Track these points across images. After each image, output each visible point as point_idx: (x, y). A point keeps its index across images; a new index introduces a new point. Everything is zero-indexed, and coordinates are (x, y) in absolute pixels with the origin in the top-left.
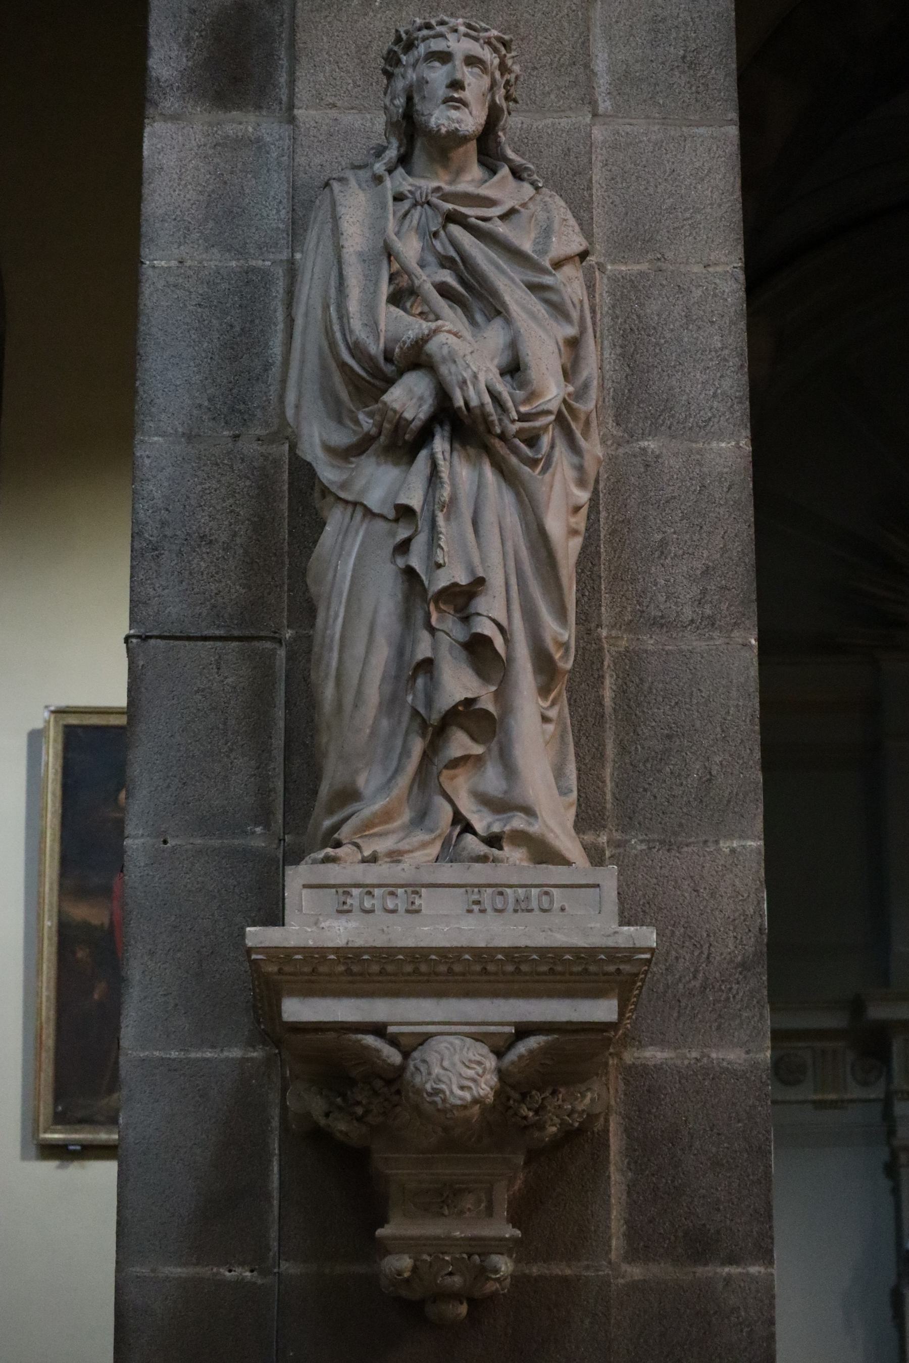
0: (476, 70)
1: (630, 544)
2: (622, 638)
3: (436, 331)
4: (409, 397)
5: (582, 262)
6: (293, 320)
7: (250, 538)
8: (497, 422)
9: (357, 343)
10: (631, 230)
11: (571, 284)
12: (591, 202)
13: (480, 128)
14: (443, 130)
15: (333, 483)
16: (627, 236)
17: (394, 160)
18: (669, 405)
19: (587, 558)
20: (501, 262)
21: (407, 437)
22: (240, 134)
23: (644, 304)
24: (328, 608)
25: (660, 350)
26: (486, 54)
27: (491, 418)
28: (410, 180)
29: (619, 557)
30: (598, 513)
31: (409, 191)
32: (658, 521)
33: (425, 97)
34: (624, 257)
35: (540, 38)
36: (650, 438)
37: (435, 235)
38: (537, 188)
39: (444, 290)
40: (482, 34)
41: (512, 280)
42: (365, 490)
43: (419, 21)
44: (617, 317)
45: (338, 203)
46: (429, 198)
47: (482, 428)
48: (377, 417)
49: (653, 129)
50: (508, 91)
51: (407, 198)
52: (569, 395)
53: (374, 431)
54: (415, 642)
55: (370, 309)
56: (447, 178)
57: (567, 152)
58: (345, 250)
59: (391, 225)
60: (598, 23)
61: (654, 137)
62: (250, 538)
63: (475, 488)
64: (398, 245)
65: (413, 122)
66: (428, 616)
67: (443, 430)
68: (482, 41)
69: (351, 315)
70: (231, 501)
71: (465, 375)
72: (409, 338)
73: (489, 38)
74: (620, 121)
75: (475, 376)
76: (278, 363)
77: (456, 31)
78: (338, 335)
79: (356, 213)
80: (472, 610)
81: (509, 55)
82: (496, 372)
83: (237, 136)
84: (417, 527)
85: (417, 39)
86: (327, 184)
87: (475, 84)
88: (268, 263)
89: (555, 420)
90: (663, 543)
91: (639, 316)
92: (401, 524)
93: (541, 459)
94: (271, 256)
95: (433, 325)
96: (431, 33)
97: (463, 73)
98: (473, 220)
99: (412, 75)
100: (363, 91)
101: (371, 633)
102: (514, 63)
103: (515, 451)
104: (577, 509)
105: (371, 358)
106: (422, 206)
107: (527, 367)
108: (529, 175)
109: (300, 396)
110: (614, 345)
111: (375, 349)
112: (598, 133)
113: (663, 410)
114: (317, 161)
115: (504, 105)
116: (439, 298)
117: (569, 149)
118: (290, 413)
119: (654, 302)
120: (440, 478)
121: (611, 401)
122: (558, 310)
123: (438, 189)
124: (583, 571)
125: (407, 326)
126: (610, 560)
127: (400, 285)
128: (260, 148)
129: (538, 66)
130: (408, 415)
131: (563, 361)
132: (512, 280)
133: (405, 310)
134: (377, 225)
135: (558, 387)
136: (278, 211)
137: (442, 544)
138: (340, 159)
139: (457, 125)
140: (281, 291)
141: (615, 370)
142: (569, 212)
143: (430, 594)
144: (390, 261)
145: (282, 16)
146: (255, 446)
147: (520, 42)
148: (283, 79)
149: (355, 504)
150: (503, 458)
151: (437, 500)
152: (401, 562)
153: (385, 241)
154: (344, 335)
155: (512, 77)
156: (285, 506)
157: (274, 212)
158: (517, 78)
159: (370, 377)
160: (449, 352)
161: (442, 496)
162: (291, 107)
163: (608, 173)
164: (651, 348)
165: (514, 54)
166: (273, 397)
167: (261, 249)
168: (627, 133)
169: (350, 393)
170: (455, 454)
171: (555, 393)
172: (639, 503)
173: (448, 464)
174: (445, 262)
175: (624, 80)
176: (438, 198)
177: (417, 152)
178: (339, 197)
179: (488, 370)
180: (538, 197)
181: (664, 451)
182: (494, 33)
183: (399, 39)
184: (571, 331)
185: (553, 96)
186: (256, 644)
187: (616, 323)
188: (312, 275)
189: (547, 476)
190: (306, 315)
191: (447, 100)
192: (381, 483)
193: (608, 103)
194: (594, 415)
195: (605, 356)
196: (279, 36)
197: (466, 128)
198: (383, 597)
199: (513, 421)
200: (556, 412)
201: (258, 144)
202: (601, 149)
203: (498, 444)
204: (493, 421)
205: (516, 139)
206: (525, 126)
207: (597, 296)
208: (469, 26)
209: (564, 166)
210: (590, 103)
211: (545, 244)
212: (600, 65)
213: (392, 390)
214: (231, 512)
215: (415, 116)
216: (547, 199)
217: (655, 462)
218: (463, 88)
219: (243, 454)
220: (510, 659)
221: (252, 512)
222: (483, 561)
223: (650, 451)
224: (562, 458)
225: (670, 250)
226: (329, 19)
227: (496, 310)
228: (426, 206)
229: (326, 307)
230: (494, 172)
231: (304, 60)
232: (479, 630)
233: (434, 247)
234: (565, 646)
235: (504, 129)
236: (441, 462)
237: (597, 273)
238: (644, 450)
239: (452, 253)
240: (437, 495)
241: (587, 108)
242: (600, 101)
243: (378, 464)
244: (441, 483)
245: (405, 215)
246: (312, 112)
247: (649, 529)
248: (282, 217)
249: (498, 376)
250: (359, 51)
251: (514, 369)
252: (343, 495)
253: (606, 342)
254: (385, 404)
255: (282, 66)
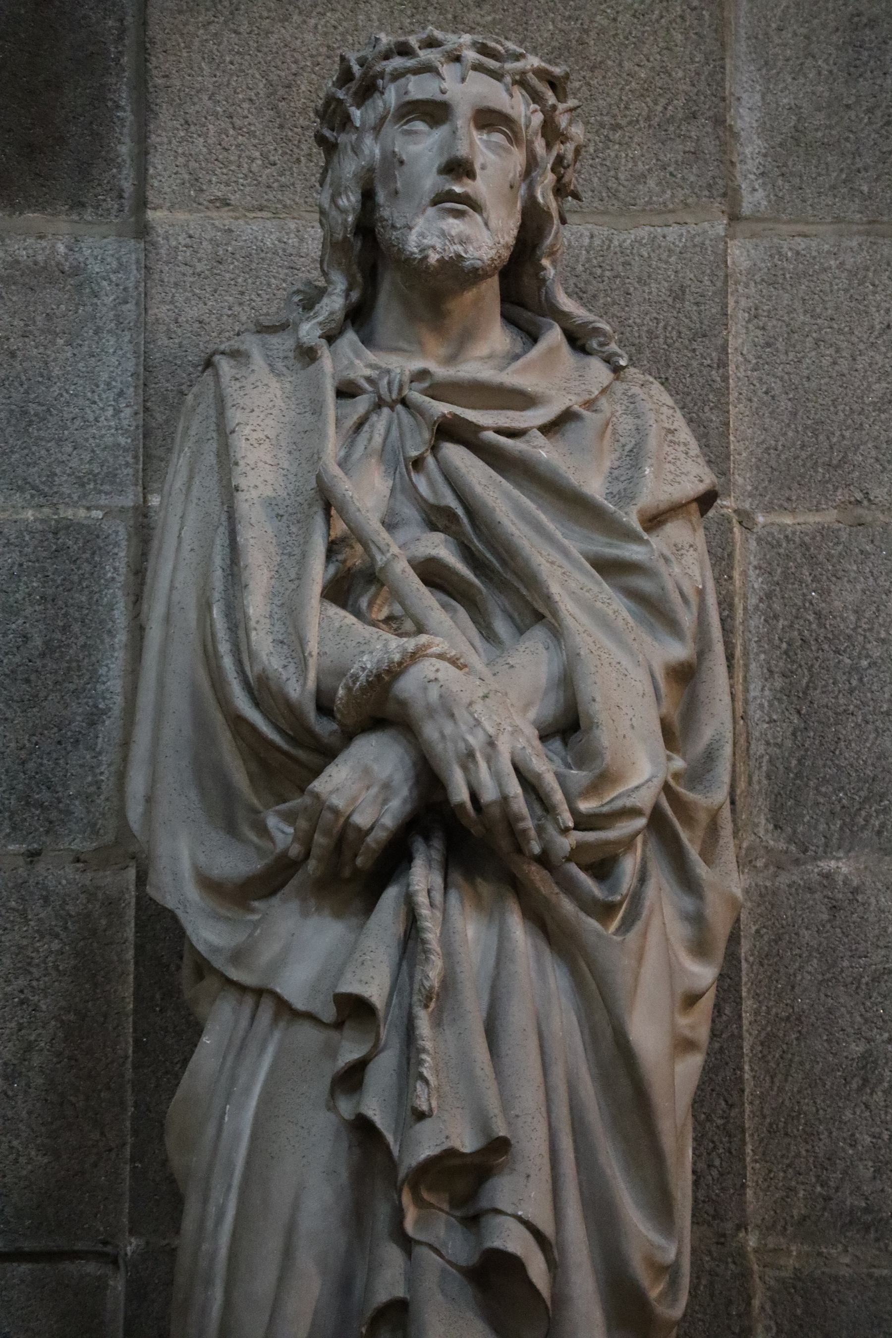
0: (497, 137)
1: (801, 1063)
2: (789, 1252)
3: (415, 656)
4: (363, 784)
5: (702, 516)
6: (142, 628)
7: (59, 1054)
8: (533, 833)
9: (264, 680)
10: (803, 447)
11: (681, 559)
12: (724, 392)
13: (506, 254)
14: (433, 258)
15: (216, 950)
16: (796, 458)
17: (340, 316)
18: (877, 788)
19: (716, 1091)
20: (543, 517)
21: (359, 861)
22: (40, 258)
23: (829, 592)
24: (205, 1201)
25: (861, 680)
26: (518, 106)
27: (521, 825)
28: (370, 356)
29: (781, 1090)
30: (739, 1001)
31: (369, 379)
32: (859, 1019)
33: (397, 193)
34: (789, 499)
35: (627, 65)
36: (841, 855)
37: (417, 464)
38: (617, 370)
39: (432, 574)
40: (509, 66)
41: (565, 553)
42: (278, 964)
43: (385, 39)
44: (776, 617)
45: (229, 402)
46: (406, 392)
47: (504, 844)
48: (303, 824)
49: (849, 243)
50: (560, 179)
51: (362, 391)
52: (676, 776)
53: (295, 850)
54: (373, 1269)
55: (290, 614)
56: (443, 351)
57: (679, 294)
58: (241, 496)
59: (332, 446)
60: (742, 32)
61: (850, 262)
62: (59, 1054)
63: (492, 962)
64: (345, 486)
65: (375, 239)
66: (399, 1214)
67: (429, 846)
68: (508, 79)
69: (253, 623)
70: (21, 982)
71: (471, 739)
72: (364, 669)
73: (523, 73)
74: (784, 228)
75: (491, 743)
76: (116, 711)
77: (458, 59)
78: (228, 662)
79: (265, 422)
80: (484, 1204)
81: (561, 107)
82: (532, 733)
83: (36, 263)
84: (378, 1039)
85: (382, 75)
86: (209, 364)
87: (495, 165)
88: (98, 514)
89: (648, 826)
90: (868, 1061)
91: (818, 614)
92: (347, 1031)
93: (621, 903)
94: (103, 501)
95: (411, 644)
96: (410, 63)
97: (472, 144)
98: (490, 435)
99: (372, 148)
100: (282, 174)
101: (288, 1253)
102: (570, 123)
103: (570, 887)
104: (691, 1000)
105: (292, 709)
106: (392, 408)
107: (593, 725)
108: (602, 345)
109: (153, 782)
110: (771, 671)
111: (299, 690)
112: (740, 254)
113: (866, 800)
114: (193, 312)
115: (553, 205)
116: (424, 589)
117: (682, 288)
118: (135, 813)
119: (848, 586)
120: (424, 942)
121: (765, 782)
122: (655, 610)
123: (422, 374)
124: (709, 1119)
125: (356, 644)
126: (762, 1097)
127: (349, 564)
128: (79, 287)
129: (623, 122)
130: (362, 819)
131: (664, 711)
132: (565, 553)
133: (358, 614)
134: (303, 444)
135: (653, 760)
136: (117, 412)
137: (426, 1073)
138: (237, 308)
139: (460, 249)
140: (123, 570)
141: (772, 721)
142: (679, 414)
143: (402, 1172)
144: (328, 517)
145: (121, 20)
146: (70, 871)
147: (588, 75)
148: (125, 149)
149: (260, 993)
150: (547, 901)
151: (416, 986)
152: (346, 1108)
153: (319, 478)
154: (239, 663)
155: (568, 149)
156: (127, 991)
157: (110, 412)
158: (577, 151)
159: (290, 744)
160: (441, 696)
161: (427, 977)
162: (142, 204)
163: (759, 333)
164: (841, 678)
165: (571, 103)
166: (106, 774)
167: (83, 485)
168: (798, 253)
169: (251, 776)
170: (453, 896)
171: (646, 776)
172: (820, 983)
173: (438, 914)
174: (436, 518)
175: (793, 145)
176: (425, 392)
177: (383, 298)
178: (231, 389)
179: (516, 731)
180: (619, 387)
181: (868, 880)
182: (534, 61)
183: (346, 76)
184: (679, 651)
185: (651, 183)
186: (70, 1267)
187: (774, 628)
188: (180, 543)
189: (632, 936)
190: (167, 619)
191: (441, 198)
192: (308, 951)
193: (760, 194)
194: (726, 813)
195: (753, 694)
196: (117, 61)
197: (477, 254)
198: (311, 1177)
199: (565, 831)
200: (648, 811)
201: (74, 278)
202: (747, 286)
203: (537, 875)
204: (524, 831)
205: (580, 268)
206: (597, 242)
207: (736, 575)
208: (483, 50)
209: (672, 321)
210: (724, 195)
211: (630, 479)
212: (745, 117)
213: (331, 769)
214: (22, 1002)
215: (379, 229)
216: (636, 390)
217: (851, 902)
218: (471, 174)
219: (45, 888)
220: (560, 1298)
221: (63, 1003)
222: (506, 1103)
223: (840, 880)
224: (664, 902)
225: (881, 484)
226: (213, 29)
227: (534, 611)
228: (399, 407)
229: (206, 607)
230: (533, 337)
231: (165, 114)
232: (497, 1244)
233: (415, 487)
234: (671, 1271)
235: (552, 254)
236: (425, 911)
237: (737, 529)
238: (827, 876)
239: (451, 501)
240: (418, 977)
241: (717, 205)
242: (745, 192)
243: (305, 914)
244: (426, 952)
245: (359, 426)
246: (181, 216)
247: (840, 1035)
248: (125, 423)
249: (537, 743)
250: (274, 93)
251: (567, 727)
252: (234, 974)
253: (753, 666)
254: (317, 796)
255: (122, 119)
